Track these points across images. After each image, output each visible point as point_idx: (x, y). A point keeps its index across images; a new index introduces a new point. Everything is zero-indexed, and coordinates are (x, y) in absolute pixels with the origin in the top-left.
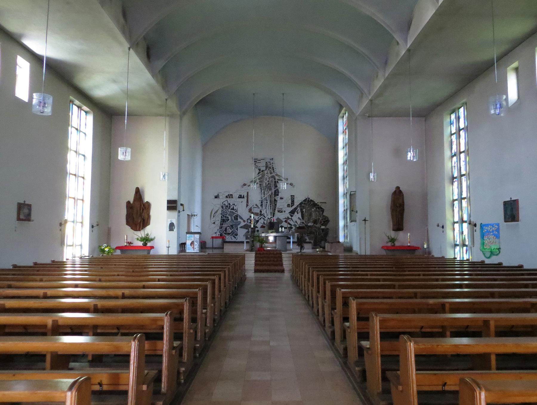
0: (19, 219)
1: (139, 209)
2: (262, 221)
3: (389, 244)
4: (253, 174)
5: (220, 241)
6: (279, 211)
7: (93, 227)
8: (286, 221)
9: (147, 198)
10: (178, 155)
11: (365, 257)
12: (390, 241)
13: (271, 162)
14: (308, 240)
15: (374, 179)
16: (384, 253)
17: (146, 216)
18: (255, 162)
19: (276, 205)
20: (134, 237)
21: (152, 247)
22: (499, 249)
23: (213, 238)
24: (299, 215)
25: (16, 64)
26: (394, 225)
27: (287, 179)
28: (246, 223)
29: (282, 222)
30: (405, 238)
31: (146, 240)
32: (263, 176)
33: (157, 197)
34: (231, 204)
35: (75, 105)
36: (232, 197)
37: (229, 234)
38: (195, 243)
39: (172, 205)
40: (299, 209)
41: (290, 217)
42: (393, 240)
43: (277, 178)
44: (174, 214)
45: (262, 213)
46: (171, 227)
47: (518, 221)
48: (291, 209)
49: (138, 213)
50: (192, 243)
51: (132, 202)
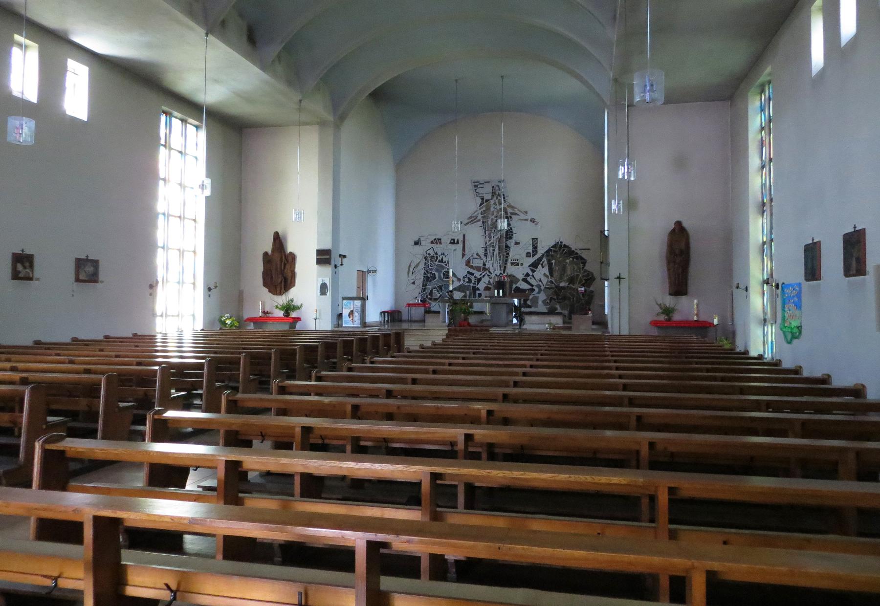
0: (78, 280)
1: (279, 263)
2: (486, 280)
3: (662, 318)
4: (473, 206)
5: (421, 310)
6: (512, 264)
7: (210, 289)
8: (525, 280)
9: (290, 248)
10: (331, 183)
11: (631, 338)
12: (663, 313)
13: (502, 185)
14: (559, 310)
15: (619, 210)
16: (655, 332)
17: (290, 275)
18: (476, 186)
19: (508, 254)
20: (273, 303)
21: (299, 319)
22: (800, 328)
23: (409, 305)
24: (546, 270)
25: (64, 69)
26: (671, 284)
27: (526, 212)
28: (462, 282)
29: (518, 280)
30: (689, 308)
31: (288, 309)
32: (488, 208)
33: (304, 247)
34: (439, 254)
35: (176, 118)
36: (440, 243)
37: (436, 299)
38: (356, 314)
39: (324, 257)
40: (544, 259)
41: (531, 273)
42: (668, 311)
43: (510, 210)
44: (328, 270)
45: (487, 267)
46: (323, 289)
47: (819, 279)
48: (531, 260)
49: (279, 270)
50: (351, 313)
51: (270, 253)
